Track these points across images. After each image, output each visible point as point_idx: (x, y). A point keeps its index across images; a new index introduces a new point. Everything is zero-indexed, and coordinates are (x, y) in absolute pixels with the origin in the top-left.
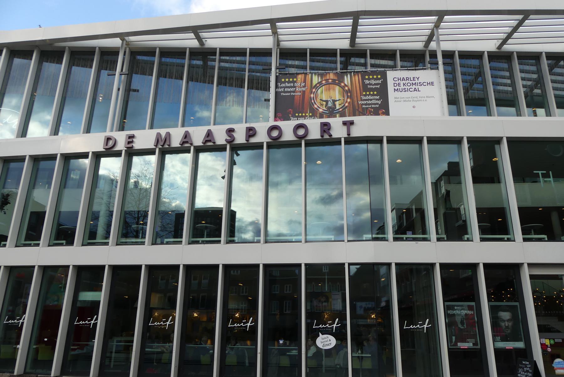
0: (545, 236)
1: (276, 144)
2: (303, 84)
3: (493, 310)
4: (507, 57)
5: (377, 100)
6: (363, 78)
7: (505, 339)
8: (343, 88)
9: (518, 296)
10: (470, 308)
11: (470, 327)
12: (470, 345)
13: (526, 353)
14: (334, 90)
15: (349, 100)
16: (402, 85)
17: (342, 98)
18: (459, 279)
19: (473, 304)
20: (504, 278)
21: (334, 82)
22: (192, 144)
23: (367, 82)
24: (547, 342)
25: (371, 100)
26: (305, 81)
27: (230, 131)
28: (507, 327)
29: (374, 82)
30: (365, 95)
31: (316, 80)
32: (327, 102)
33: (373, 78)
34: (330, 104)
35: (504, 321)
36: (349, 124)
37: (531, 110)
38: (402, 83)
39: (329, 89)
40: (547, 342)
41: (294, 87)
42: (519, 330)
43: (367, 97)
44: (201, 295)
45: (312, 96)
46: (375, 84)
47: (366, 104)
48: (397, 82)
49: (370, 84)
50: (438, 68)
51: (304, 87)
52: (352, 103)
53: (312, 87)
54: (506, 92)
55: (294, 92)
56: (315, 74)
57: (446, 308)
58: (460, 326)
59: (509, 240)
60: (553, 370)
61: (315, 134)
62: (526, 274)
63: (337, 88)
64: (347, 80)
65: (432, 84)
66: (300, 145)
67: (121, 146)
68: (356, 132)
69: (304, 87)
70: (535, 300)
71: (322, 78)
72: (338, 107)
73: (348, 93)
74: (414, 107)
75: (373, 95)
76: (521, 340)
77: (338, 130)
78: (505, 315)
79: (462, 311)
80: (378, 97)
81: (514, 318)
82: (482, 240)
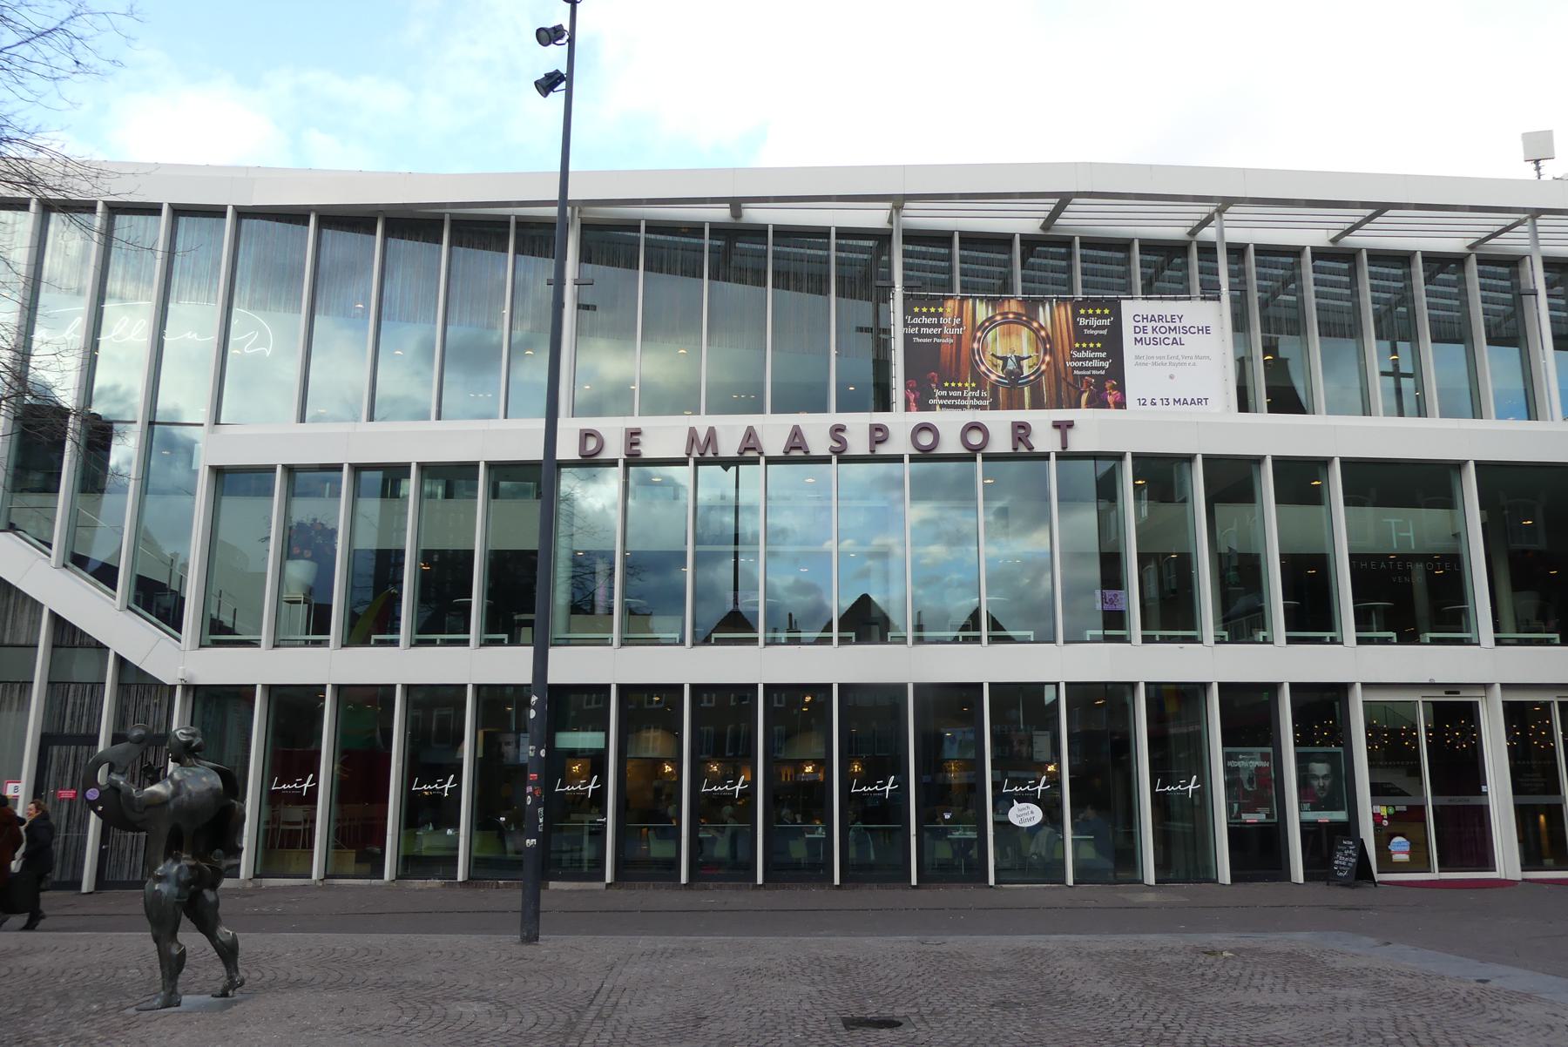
0: (1393, 634)
1: (925, 455)
2: (957, 321)
3: (1302, 760)
4: (1351, 256)
5: (1102, 359)
6: (1076, 314)
7: (1314, 808)
8: (1036, 332)
9: (1341, 735)
10: (1265, 757)
11: (1256, 790)
12: (1262, 817)
13: (1349, 829)
14: (1019, 335)
15: (1047, 358)
16: (1149, 330)
17: (1034, 354)
18: (1249, 708)
19: (1269, 750)
20: (1321, 706)
21: (1018, 320)
22: (761, 453)
23: (1083, 321)
24: (1383, 811)
25: (1091, 359)
26: (960, 315)
27: (838, 430)
28: (1323, 788)
29: (1096, 323)
30: (1079, 350)
31: (983, 312)
32: (1005, 359)
33: (1094, 315)
34: (1011, 365)
35: (1317, 777)
36: (1063, 427)
37: (1386, 344)
38: (1150, 325)
39: (1009, 334)
40: (1383, 811)
41: (939, 325)
42: (1340, 792)
43: (1083, 354)
44: (435, 713)
45: (976, 346)
46: (1098, 327)
47: (1081, 369)
48: (1141, 324)
49: (1089, 327)
50: (1218, 299)
51: (960, 326)
52: (1054, 364)
53: (975, 329)
54: (1340, 311)
55: (939, 336)
56: (981, 299)
57: (1227, 757)
58: (1246, 786)
59: (1333, 641)
60: (1390, 855)
61: (1001, 442)
62: (1357, 701)
63: (1025, 331)
64: (1044, 315)
65: (1207, 330)
66: (974, 459)
67: (615, 449)
68: (1077, 444)
69: (960, 326)
70: (1369, 741)
71: (994, 309)
72: (1026, 373)
73: (1045, 342)
74: (1171, 377)
75: (1095, 350)
76: (1342, 809)
77: (1045, 440)
78: (1320, 769)
79: (1251, 761)
80: (1103, 355)
81: (1335, 772)
82: (1290, 640)
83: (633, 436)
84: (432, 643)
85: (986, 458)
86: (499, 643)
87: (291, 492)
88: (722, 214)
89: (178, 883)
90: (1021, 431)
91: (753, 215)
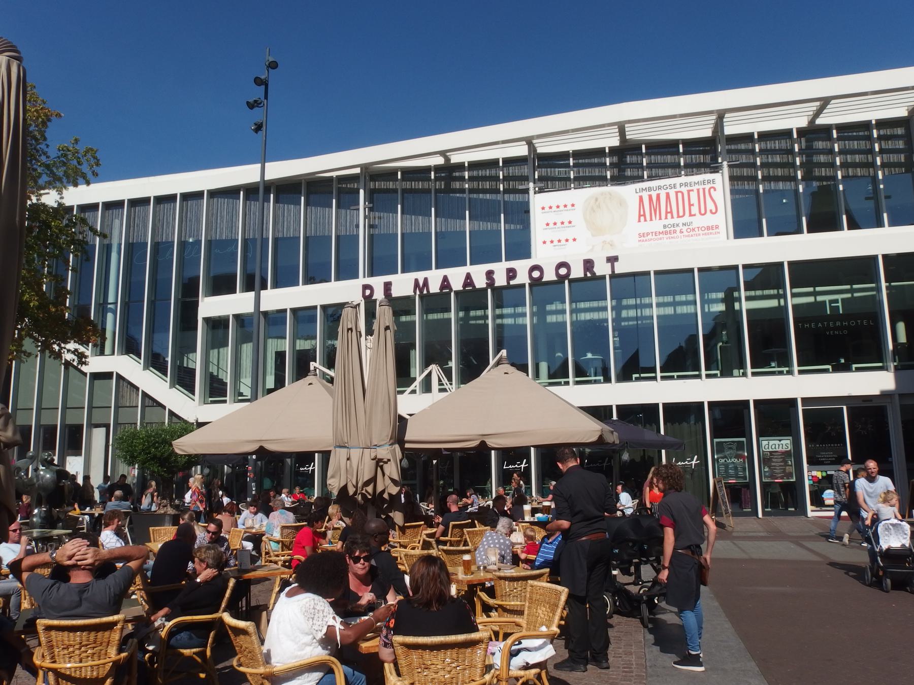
27: (490, 274)
83: (388, 286)
84: (672, 378)
85: (571, 281)
86: (715, 376)
87: (498, 304)
88: (440, 161)
89: (41, 517)
90: (468, 279)
91: (455, 158)
